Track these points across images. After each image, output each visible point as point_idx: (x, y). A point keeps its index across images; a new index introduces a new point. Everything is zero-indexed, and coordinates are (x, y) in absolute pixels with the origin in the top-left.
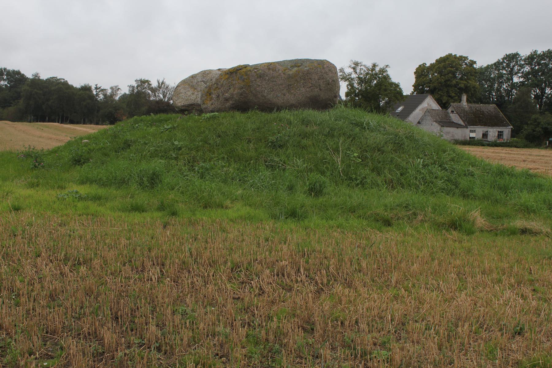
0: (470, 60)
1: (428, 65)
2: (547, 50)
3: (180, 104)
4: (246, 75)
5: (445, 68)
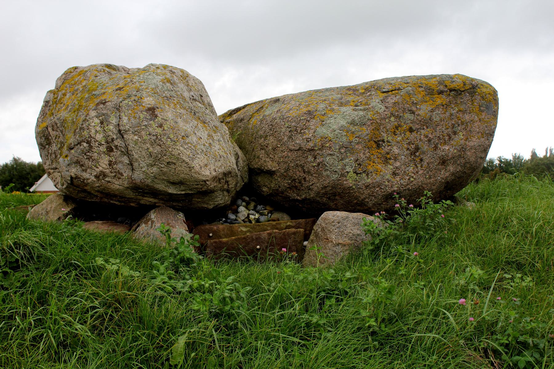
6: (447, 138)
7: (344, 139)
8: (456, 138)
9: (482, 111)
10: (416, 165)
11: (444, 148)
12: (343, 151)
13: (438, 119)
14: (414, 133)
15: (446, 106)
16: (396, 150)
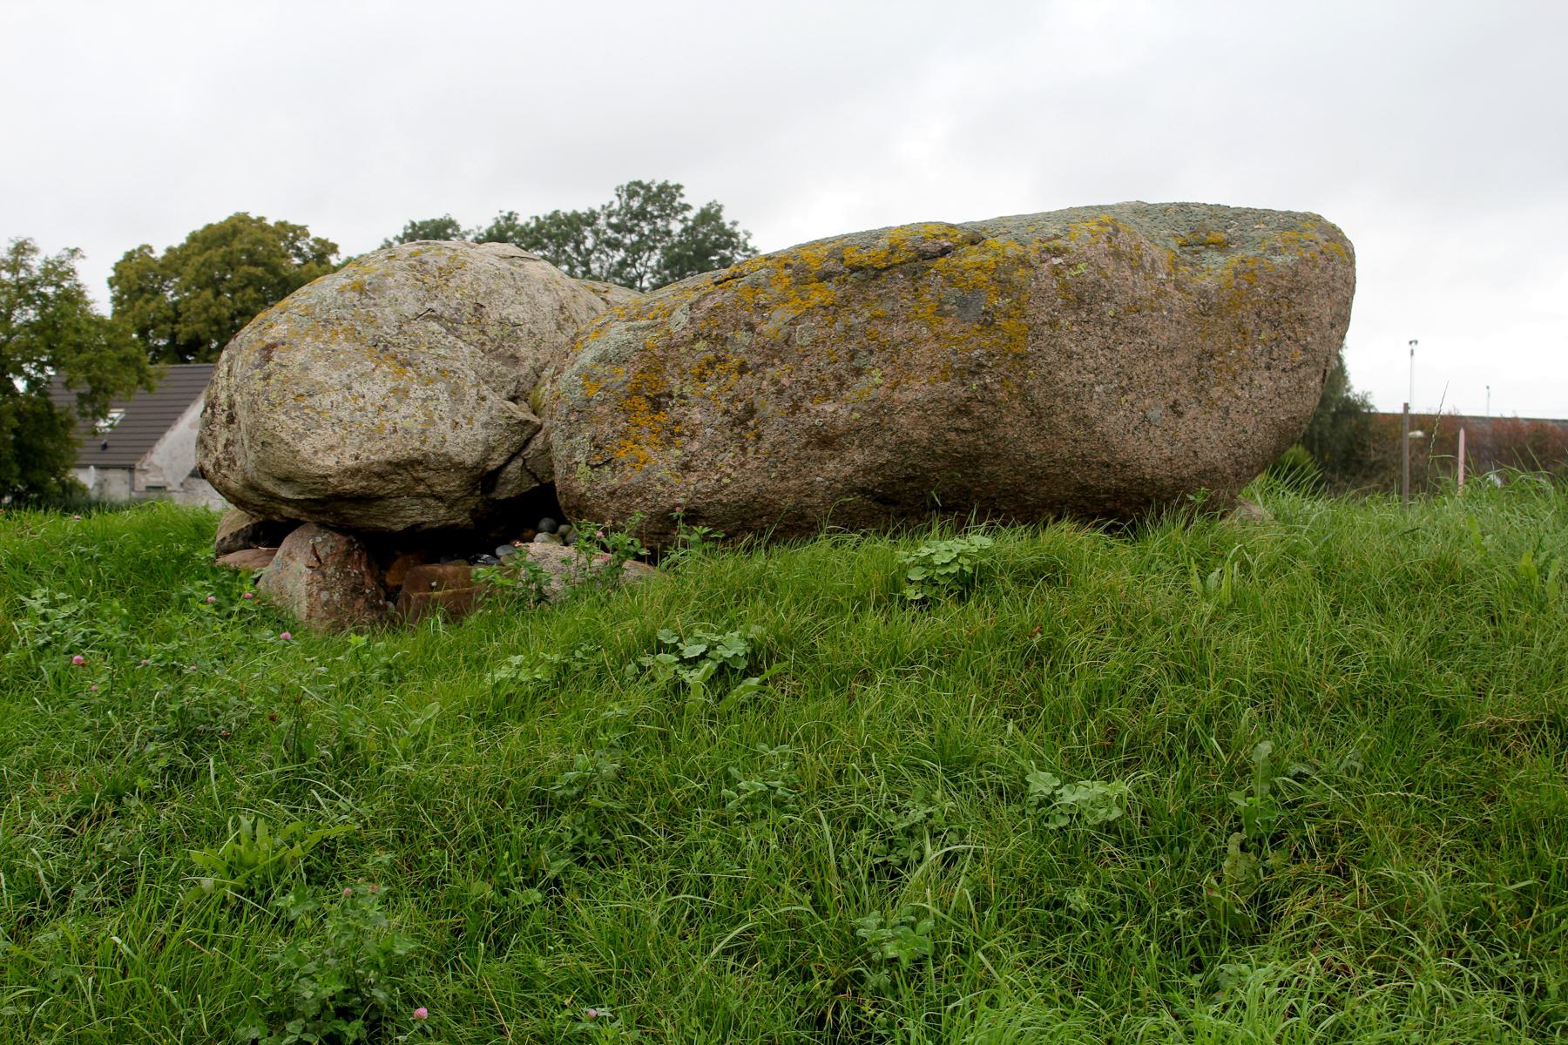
0: (317, 241)
1: (159, 253)
2: (549, 213)
3: (329, 462)
4: (1004, 285)
5: (230, 265)
6: (832, 385)
7: (578, 393)
8: (861, 385)
9: (946, 314)
10: (743, 449)
11: (819, 408)
12: (573, 418)
13: (807, 340)
14: (747, 377)
15: (832, 310)
16: (697, 416)
